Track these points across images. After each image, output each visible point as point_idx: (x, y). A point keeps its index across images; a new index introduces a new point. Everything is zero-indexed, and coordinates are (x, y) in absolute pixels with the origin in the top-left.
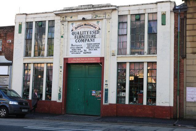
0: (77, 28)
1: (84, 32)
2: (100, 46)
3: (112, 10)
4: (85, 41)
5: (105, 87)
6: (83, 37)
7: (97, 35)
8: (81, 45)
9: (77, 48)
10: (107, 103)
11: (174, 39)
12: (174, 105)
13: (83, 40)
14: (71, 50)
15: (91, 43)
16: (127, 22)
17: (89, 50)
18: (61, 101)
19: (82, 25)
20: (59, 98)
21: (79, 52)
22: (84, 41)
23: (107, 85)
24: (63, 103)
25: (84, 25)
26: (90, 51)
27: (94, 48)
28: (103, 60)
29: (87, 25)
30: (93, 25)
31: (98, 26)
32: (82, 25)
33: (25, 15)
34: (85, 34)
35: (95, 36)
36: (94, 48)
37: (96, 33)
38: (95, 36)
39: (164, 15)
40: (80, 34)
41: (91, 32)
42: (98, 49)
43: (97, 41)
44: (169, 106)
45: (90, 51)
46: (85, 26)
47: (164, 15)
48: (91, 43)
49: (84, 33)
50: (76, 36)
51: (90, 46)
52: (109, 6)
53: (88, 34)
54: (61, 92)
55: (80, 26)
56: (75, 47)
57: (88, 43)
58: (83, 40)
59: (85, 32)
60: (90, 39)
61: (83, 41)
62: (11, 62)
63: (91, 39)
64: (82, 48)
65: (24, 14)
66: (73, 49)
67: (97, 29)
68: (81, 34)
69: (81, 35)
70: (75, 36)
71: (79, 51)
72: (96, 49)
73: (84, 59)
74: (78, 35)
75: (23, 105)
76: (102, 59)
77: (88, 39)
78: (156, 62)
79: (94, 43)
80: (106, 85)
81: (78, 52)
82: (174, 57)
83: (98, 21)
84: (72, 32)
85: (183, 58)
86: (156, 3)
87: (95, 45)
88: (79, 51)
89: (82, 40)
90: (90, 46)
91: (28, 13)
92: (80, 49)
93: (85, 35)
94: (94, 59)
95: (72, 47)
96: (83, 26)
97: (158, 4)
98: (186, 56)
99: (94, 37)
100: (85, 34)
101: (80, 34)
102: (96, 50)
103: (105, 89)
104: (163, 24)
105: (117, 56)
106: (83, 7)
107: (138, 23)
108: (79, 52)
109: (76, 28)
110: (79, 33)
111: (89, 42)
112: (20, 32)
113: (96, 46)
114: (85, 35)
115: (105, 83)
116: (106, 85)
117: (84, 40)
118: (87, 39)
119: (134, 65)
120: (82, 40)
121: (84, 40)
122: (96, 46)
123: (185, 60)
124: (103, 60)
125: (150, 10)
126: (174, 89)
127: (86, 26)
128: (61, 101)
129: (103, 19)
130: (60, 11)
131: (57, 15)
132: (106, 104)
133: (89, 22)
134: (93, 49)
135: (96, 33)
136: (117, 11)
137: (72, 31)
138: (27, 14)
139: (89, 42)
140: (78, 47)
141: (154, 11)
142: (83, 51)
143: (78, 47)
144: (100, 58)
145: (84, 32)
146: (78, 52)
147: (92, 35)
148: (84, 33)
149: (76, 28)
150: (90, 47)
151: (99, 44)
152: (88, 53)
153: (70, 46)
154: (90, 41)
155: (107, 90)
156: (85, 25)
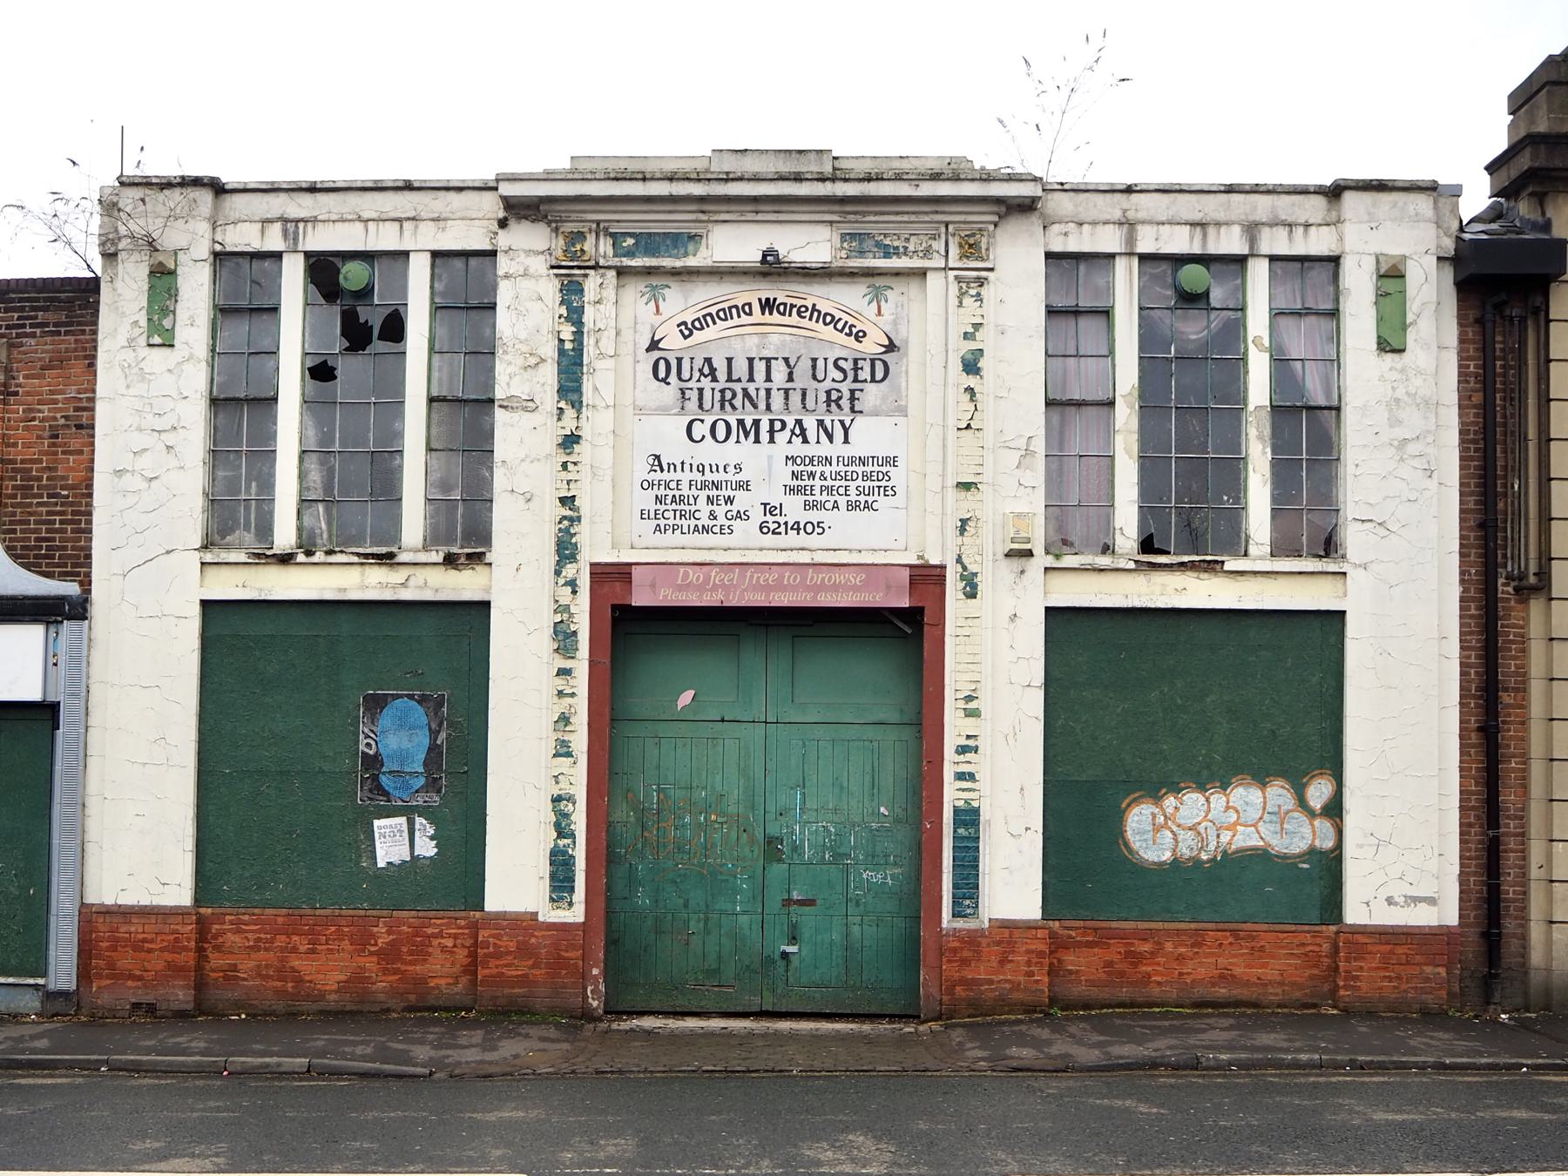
0: (701, 323)
1: (760, 367)
2: (897, 476)
3: (1003, 209)
4: (772, 432)
5: (952, 795)
6: (755, 406)
7: (872, 395)
8: (738, 468)
9: (704, 486)
10: (975, 914)
11: (1462, 458)
12: (1460, 917)
13: (756, 423)
14: (647, 500)
15: (825, 449)
16: (1106, 313)
17: (808, 506)
18: (575, 913)
19: (746, 309)
20: (561, 881)
21: (721, 520)
22: (765, 436)
23: (971, 777)
24: (1473, 935)
25: (756, 308)
26: (814, 516)
27: (853, 491)
28: (937, 589)
29: (786, 310)
30: (838, 315)
31: (880, 321)
32: (746, 309)
33: (205, 197)
34: (768, 379)
35: (853, 399)
36: (853, 491)
37: (865, 374)
38: (853, 399)
39: (1391, 275)
40: (722, 374)
41: (820, 363)
42: (882, 502)
43: (869, 436)
44: (1435, 923)
45: (814, 516)
46: (767, 318)
47: (1391, 275)
48: (825, 449)
49: (760, 374)
50: (694, 395)
51: (812, 475)
52: (956, 178)
53: (790, 379)
54: (573, 836)
55: (725, 315)
56: (686, 477)
57: (797, 448)
58: (748, 423)
59: (768, 360)
60: (810, 423)
61: (751, 431)
62: (71, 589)
63: (821, 423)
64: (744, 486)
65: (197, 182)
66: (662, 492)
67: (871, 347)
68: (729, 380)
69: (738, 387)
70: (683, 391)
71: (720, 511)
72: (862, 498)
73: (771, 577)
74: (706, 383)
75: (75, 426)
76: (927, 578)
77: (799, 422)
78: (1345, 612)
79: (847, 451)
80: (960, 776)
81: (713, 516)
82: (1462, 581)
83: (879, 282)
84: (656, 354)
85: (1524, 592)
86: (1335, 192)
87: (860, 469)
88: (720, 511)
89: (741, 422)
90: (812, 475)
91: (228, 177)
92: (729, 500)
93: (768, 391)
94: (856, 578)
95: (658, 476)
96: (745, 319)
97: (1349, 198)
98: (1544, 575)
99: (845, 403)
100: (768, 379)
101: (722, 374)
102: (868, 506)
103: (956, 811)
104: (1389, 345)
105: (1041, 560)
106: (750, 166)
107: (1193, 329)
108: (721, 520)
109: (687, 330)
110: (713, 371)
111: (805, 441)
112: (161, 334)
113: (867, 477)
114: (768, 391)
115: (951, 764)
116: (960, 776)
117: (765, 426)
118: (790, 423)
119: (893, 716)
120: (741, 422)
121: (765, 426)
122: (867, 477)
123: (1536, 606)
124: (937, 589)
125: (1282, 232)
126: (1461, 808)
127: (776, 318)
128: (575, 913)
129: (922, 273)
130: (549, 177)
131: (519, 210)
132: (960, 924)
133: (800, 288)
134: (842, 501)
135: (865, 374)
136: (1034, 222)
137: (654, 345)
138: (218, 188)
139: (805, 441)
140: (716, 477)
141: (1318, 243)
142: (757, 515)
143: (709, 476)
144: (906, 573)
145: (760, 367)
146: (713, 516)
147: (828, 393)
148: (760, 374)
149: (687, 330)
150: (818, 483)
151: (892, 461)
152: (797, 527)
153: (642, 471)
154: (811, 434)
155: (968, 818)
156: (768, 305)
